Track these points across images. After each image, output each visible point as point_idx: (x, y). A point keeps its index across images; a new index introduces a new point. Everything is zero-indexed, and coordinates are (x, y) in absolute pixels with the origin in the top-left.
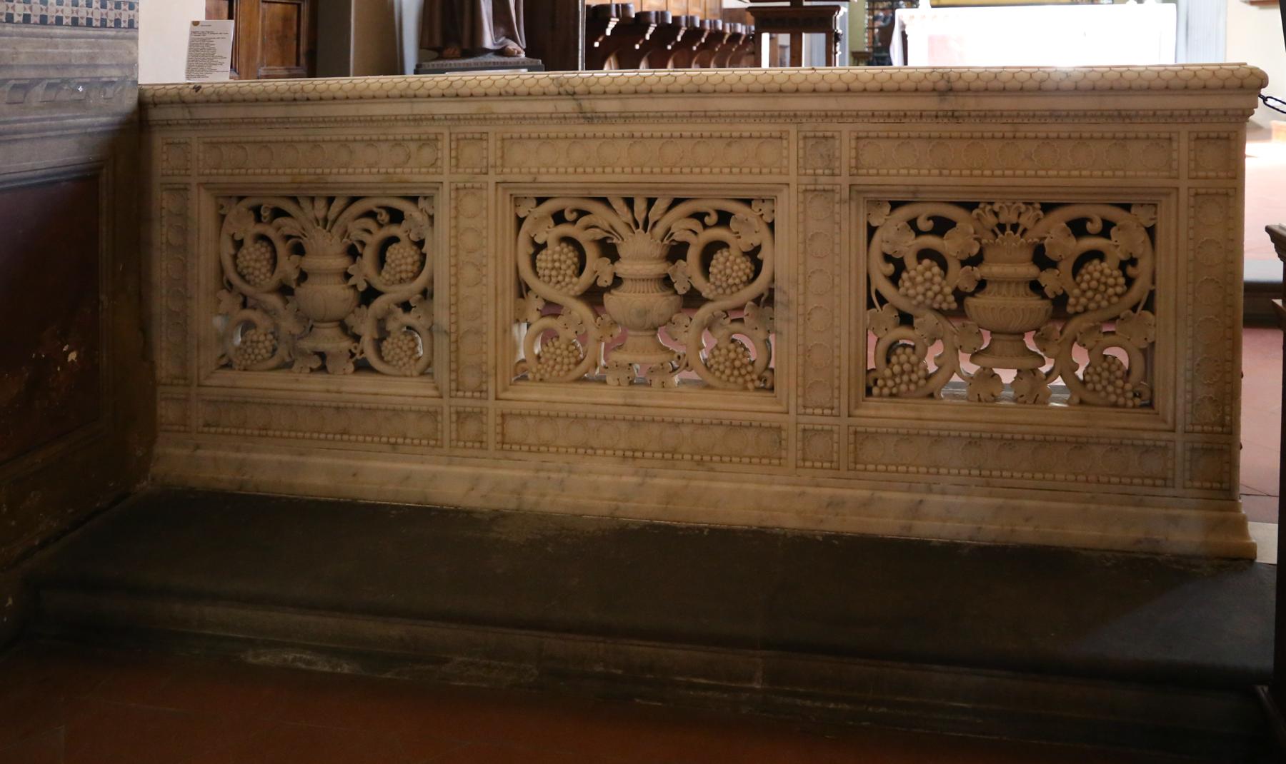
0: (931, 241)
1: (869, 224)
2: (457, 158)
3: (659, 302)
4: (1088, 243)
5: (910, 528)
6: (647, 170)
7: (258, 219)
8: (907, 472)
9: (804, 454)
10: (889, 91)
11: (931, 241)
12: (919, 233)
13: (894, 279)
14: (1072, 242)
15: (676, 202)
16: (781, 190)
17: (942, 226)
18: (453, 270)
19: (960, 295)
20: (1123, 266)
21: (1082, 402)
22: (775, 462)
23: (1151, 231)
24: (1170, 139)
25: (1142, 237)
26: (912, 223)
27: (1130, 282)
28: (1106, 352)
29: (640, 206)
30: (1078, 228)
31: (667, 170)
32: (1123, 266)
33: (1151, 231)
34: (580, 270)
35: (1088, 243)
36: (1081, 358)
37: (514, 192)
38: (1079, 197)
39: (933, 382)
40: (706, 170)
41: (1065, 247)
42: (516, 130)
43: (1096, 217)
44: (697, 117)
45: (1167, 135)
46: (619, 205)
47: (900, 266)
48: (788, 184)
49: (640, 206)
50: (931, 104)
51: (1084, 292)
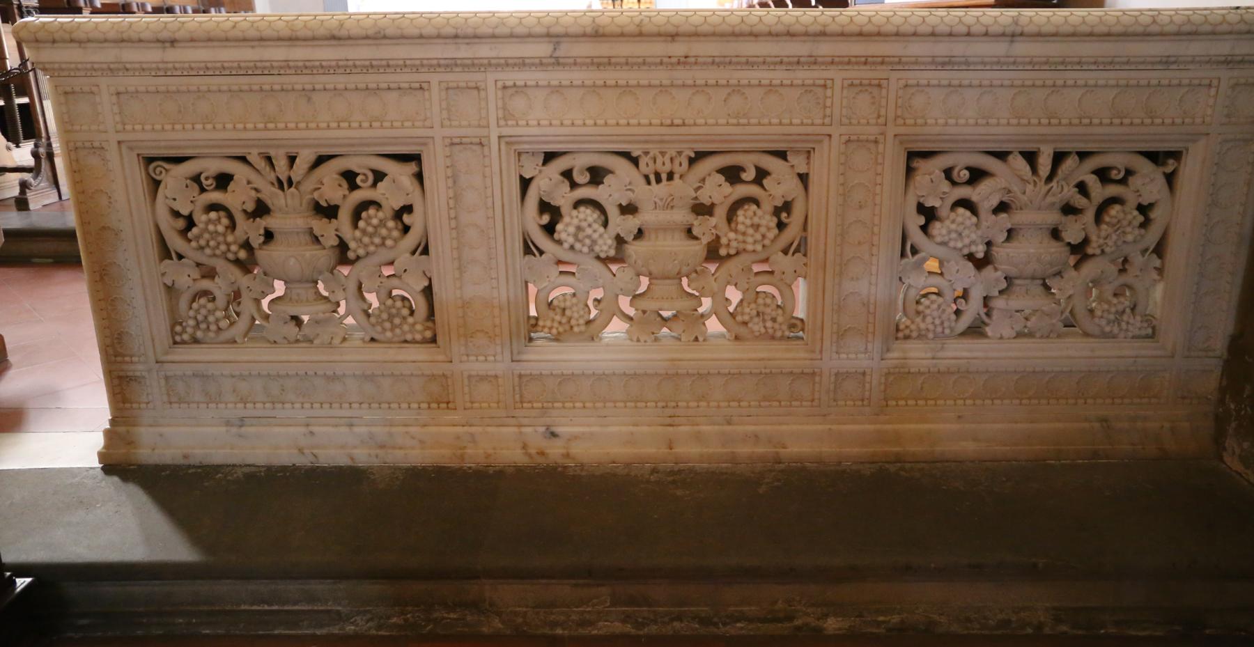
0: (216, 196)
1: (521, 177)
2: (449, 110)
3: (1055, 251)
4: (742, 190)
5: (462, 457)
6: (148, 127)
7: (574, 185)
8: (688, 407)
9: (521, 396)
10: (705, 35)
11: (216, 196)
12: (954, 184)
13: (184, 233)
14: (727, 188)
15: (321, 160)
16: (820, 142)
17: (977, 175)
18: (454, 234)
19: (620, 241)
20: (777, 211)
21: (737, 338)
22: (444, 405)
23: (804, 178)
24: (825, 86)
25: (796, 182)
26: (567, 174)
27: (781, 226)
28: (758, 289)
29: (281, 164)
30: (732, 174)
31: (303, 125)
32: (777, 211)
33: (804, 178)
34: (605, 224)
35: (742, 190)
36: (734, 295)
37: (517, 147)
38: (207, 151)
39: (593, 326)
40: (178, 127)
41: (719, 192)
42: (520, 77)
43: (749, 163)
44: (616, 64)
45: (822, 82)
46: (261, 164)
47: (190, 222)
48: (830, 136)
49: (281, 164)
50: (657, 49)
51: (228, 245)
